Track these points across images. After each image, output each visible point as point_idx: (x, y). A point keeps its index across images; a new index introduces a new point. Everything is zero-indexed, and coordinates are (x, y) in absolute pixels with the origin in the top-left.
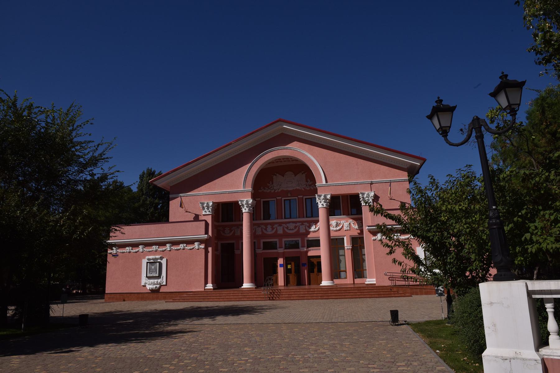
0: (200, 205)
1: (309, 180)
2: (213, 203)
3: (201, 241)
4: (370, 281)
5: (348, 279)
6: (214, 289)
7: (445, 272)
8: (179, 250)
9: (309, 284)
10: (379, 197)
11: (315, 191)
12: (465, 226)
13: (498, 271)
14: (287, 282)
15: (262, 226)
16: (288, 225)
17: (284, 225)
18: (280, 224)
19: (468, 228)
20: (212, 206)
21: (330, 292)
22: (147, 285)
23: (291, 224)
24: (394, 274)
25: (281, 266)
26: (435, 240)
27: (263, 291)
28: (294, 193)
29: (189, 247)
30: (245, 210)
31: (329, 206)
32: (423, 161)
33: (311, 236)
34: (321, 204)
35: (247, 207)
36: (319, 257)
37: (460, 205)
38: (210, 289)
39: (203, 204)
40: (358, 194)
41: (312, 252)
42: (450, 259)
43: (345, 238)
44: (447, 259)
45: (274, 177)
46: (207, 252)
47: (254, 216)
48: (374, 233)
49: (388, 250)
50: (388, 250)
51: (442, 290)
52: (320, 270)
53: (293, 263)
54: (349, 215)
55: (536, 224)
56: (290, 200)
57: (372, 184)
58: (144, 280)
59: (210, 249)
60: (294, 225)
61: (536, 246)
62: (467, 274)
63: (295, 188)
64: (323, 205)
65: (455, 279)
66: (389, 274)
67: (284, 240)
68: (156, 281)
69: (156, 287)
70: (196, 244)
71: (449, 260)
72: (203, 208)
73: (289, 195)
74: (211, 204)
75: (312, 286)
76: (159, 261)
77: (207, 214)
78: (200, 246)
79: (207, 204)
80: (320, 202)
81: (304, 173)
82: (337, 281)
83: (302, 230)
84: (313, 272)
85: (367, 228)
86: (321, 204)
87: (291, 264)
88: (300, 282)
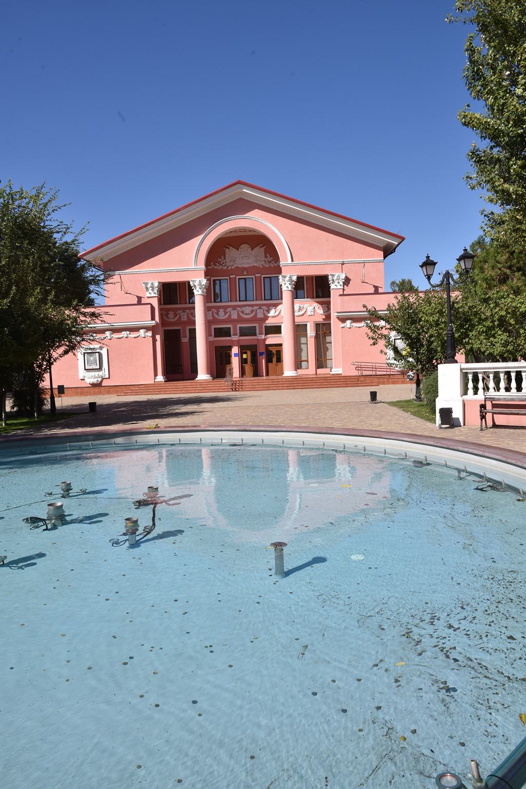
0: (144, 285)
1: (268, 255)
2: (159, 283)
3: (147, 329)
4: (337, 370)
5: (310, 369)
6: (165, 381)
7: (418, 360)
8: (121, 338)
9: (267, 374)
10: (350, 280)
11: (279, 270)
12: (435, 332)
13: (236, 346)
14: (243, 373)
15: (214, 310)
16: (243, 308)
17: (239, 309)
18: (234, 308)
19: (436, 333)
20: (158, 287)
21: (295, 382)
22: (86, 379)
23: (247, 307)
24: (362, 364)
25: (236, 355)
26: (413, 337)
27: (221, 382)
28: (252, 270)
29: (116, 336)
30: (198, 292)
31: (294, 288)
32: (401, 240)
33: (270, 322)
34: (286, 286)
35: (200, 289)
36: (281, 345)
37: (433, 317)
38: (161, 382)
39: (146, 284)
40: (328, 275)
41: (272, 340)
42: (423, 350)
43: (308, 324)
44: (420, 350)
45: (227, 250)
46: (154, 341)
47: (207, 298)
48: (343, 320)
49: (372, 341)
50: (372, 341)
51: (413, 375)
52: (279, 360)
53: (249, 352)
54: (313, 298)
55: (473, 333)
56: (245, 279)
57: (343, 264)
58: (82, 373)
59: (158, 337)
60: (251, 308)
61: (471, 346)
62: (434, 361)
63: (252, 265)
64: (287, 287)
65: (424, 365)
66: (357, 364)
67: (239, 326)
68: (96, 373)
69: (97, 381)
70: (142, 331)
71: (421, 352)
72: (147, 289)
73: (245, 273)
74: (156, 284)
75: (271, 377)
76: (98, 351)
77: (152, 296)
78: (146, 334)
79: (152, 284)
80: (285, 284)
81: (263, 246)
82: (300, 372)
83: (260, 315)
84: (272, 362)
85: (336, 314)
86: (286, 286)
87: (246, 353)
88: (256, 374)
